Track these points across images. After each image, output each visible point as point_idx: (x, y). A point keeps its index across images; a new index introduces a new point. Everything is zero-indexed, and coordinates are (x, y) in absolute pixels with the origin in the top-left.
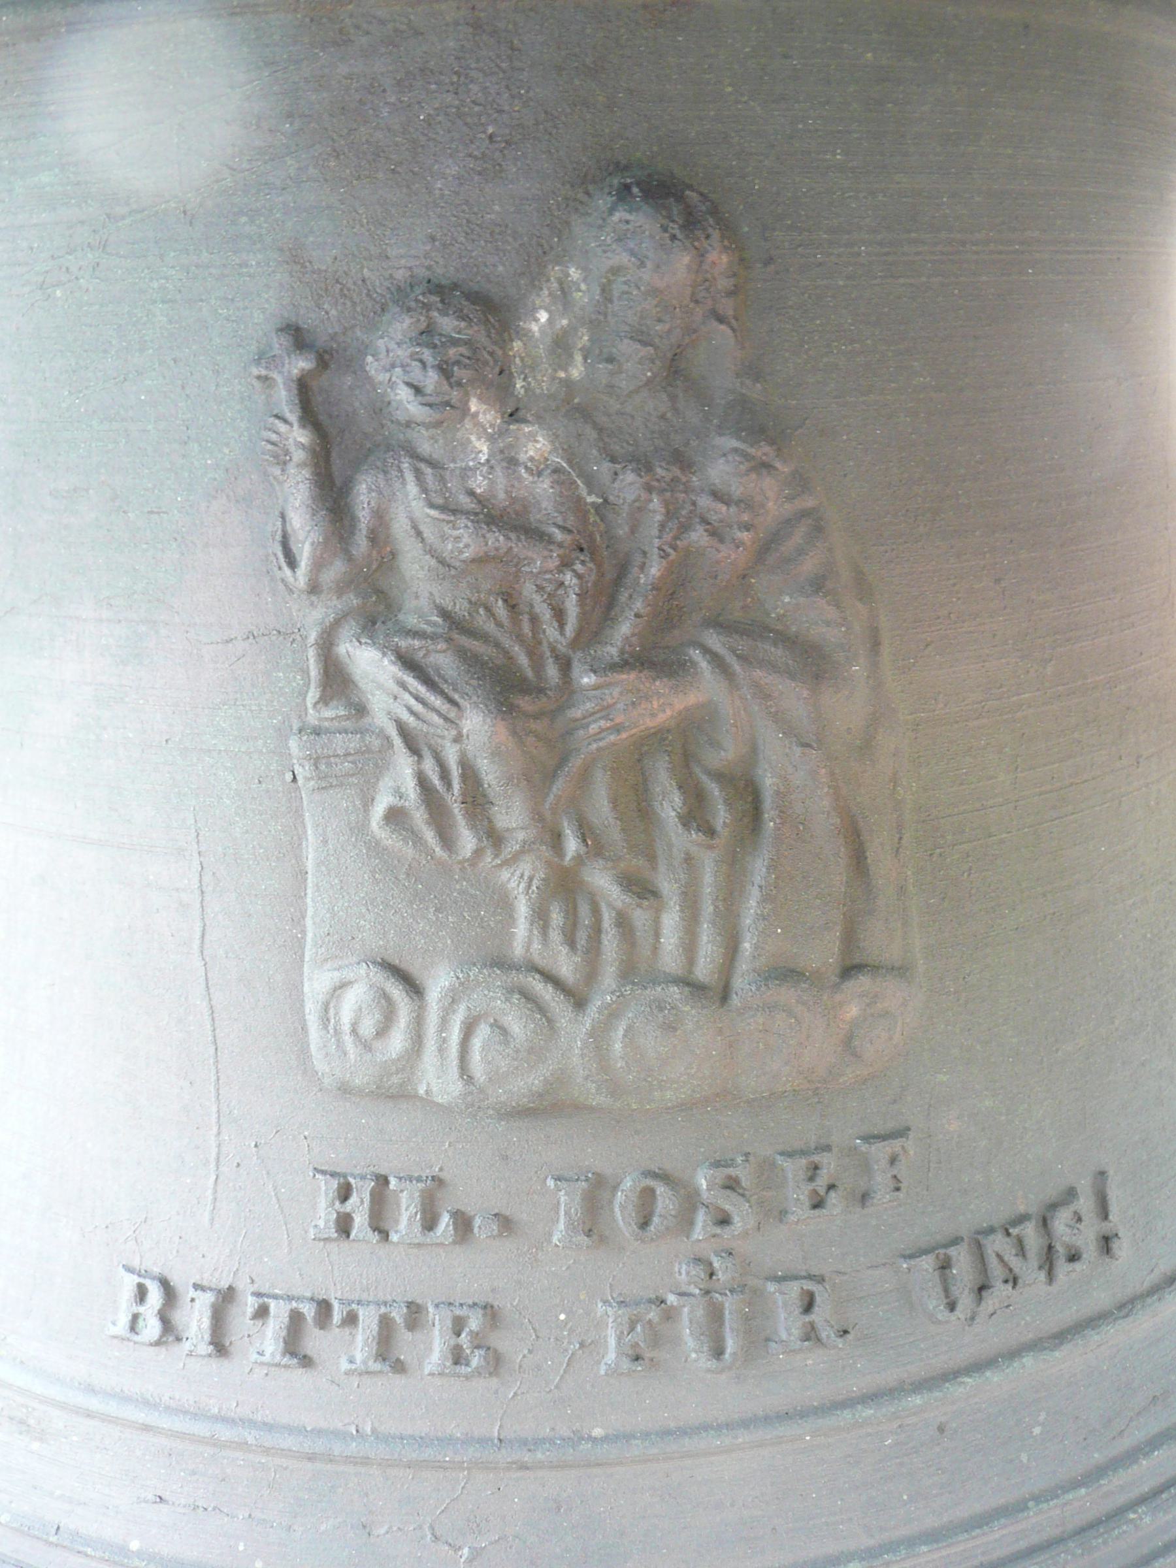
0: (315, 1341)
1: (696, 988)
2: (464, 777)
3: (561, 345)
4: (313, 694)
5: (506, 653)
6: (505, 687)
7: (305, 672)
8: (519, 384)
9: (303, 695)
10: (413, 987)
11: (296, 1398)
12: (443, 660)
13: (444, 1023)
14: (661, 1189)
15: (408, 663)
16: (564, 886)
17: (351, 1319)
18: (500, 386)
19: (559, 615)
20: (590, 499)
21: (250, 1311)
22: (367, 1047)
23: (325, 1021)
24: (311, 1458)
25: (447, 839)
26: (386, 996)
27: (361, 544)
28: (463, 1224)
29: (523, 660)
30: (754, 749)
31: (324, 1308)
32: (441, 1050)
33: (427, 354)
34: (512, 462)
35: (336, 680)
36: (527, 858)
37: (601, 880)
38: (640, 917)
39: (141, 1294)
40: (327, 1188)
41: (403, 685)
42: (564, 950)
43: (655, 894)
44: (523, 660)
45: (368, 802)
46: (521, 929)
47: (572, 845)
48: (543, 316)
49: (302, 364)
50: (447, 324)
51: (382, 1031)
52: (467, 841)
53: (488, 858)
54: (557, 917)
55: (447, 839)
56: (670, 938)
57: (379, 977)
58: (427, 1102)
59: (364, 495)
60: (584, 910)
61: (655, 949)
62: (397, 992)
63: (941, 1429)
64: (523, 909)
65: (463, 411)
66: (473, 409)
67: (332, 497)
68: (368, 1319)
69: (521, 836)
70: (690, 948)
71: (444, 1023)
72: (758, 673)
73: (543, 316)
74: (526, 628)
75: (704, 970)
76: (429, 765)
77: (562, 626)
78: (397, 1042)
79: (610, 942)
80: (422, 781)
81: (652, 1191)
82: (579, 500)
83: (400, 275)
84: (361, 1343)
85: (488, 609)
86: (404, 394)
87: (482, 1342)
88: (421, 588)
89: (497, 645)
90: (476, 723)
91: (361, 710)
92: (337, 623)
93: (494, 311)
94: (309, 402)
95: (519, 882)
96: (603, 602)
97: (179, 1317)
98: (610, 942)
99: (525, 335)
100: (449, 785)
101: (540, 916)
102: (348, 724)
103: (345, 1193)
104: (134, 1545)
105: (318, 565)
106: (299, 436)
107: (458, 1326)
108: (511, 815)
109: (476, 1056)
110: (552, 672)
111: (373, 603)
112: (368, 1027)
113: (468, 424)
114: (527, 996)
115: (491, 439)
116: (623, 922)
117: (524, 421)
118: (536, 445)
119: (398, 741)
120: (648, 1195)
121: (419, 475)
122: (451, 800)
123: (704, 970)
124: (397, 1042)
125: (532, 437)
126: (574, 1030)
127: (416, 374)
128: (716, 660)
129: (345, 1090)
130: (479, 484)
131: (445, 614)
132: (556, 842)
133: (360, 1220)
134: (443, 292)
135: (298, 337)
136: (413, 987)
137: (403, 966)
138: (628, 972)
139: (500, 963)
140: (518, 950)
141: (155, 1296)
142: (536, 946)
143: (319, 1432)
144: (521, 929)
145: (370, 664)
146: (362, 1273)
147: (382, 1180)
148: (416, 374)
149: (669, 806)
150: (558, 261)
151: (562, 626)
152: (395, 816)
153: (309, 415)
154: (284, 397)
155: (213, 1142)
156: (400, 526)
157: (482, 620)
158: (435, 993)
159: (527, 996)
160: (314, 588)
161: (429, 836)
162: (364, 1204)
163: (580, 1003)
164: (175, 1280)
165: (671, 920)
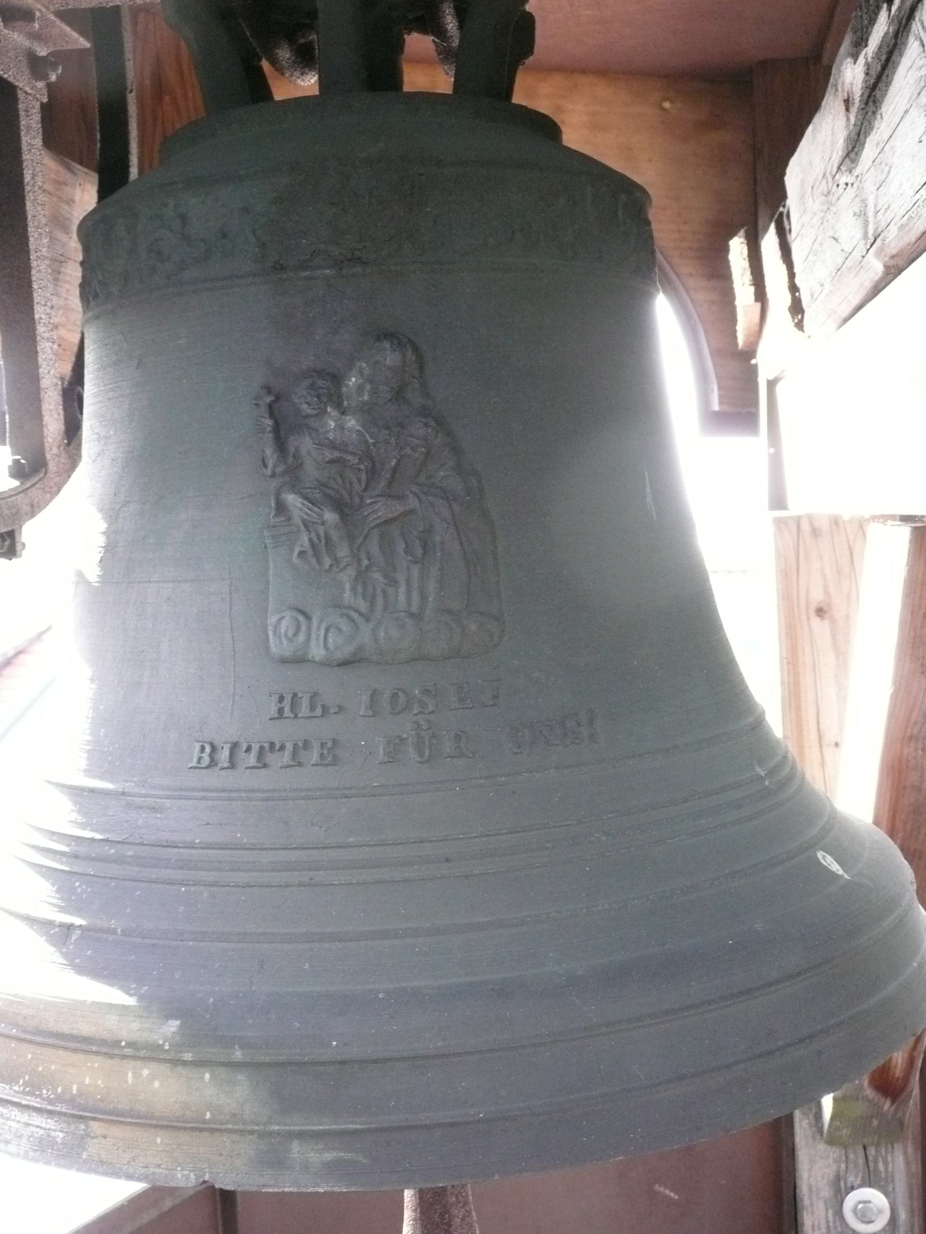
0: (270, 758)
1: (412, 615)
2: (326, 538)
3: (360, 388)
4: (273, 513)
5: (341, 495)
6: (340, 507)
7: (270, 507)
8: (346, 403)
9: (269, 515)
10: (308, 617)
11: (262, 780)
12: (317, 495)
13: (319, 628)
14: (400, 694)
15: (306, 498)
16: (361, 577)
17: (282, 748)
18: (339, 406)
19: (359, 480)
20: (371, 441)
21: (244, 748)
22: (290, 640)
23: (275, 633)
24: (266, 800)
25: (319, 562)
26: (297, 620)
27: (290, 460)
28: (325, 709)
29: (347, 496)
30: (431, 526)
31: (272, 745)
32: (317, 639)
33: (313, 393)
34: (342, 428)
35: (281, 508)
36: (349, 568)
37: (377, 576)
38: (390, 590)
39: (203, 749)
40: (275, 698)
41: (304, 504)
42: (362, 601)
43: (396, 582)
44: (347, 496)
45: (292, 551)
46: (347, 595)
47: (365, 562)
48: (354, 379)
49: (269, 399)
50: (320, 382)
51: (296, 634)
52: (327, 562)
53: (335, 569)
54: (360, 589)
55: (319, 562)
56: (402, 598)
57: (294, 613)
58: (313, 662)
59: (293, 443)
60: (370, 588)
61: (397, 601)
62: (301, 618)
63: (514, 793)
64: (348, 587)
65: (325, 411)
66: (329, 410)
67: (281, 445)
68: (289, 746)
69: (346, 559)
70: (409, 601)
71: (319, 628)
72: (430, 498)
73: (354, 379)
74: (348, 485)
75: (414, 609)
76: (313, 535)
77: (360, 485)
78: (301, 637)
79: (380, 600)
80: (311, 540)
81: (397, 694)
82: (367, 441)
83: (305, 368)
84: (286, 757)
85: (334, 479)
86: (305, 406)
87: (331, 754)
88: (311, 472)
89: (338, 492)
90: (330, 516)
91: (289, 519)
92: (281, 487)
93: (337, 379)
94: (271, 410)
95: (346, 577)
96: (373, 473)
97: (217, 757)
98: (380, 600)
99: (347, 386)
100: (320, 541)
101: (353, 589)
102: (285, 524)
103: (281, 699)
104: (197, 841)
105: (275, 467)
106: (269, 422)
107: (323, 745)
108: (343, 551)
109: (330, 640)
110: (357, 500)
111: (292, 475)
112: (290, 633)
113: (327, 415)
114: (349, 617)
115: (335, 421)
116: (384, 592)
117: (348, 415)
118: (351, 422)
119: (302, 527)
120: (395, 695)
121: (310, 435)
122: (321, 547)
123: (414, 609)
124: (301, 637)
125: (350, 420)
126: (366, 630)
127: (309, 399)
128: (415, 494)
129: (283, 661)
130: (331, 436)
131: (318, 481)
132: (359, 561)
133: (287, 712)
134: (320, 373)
135: (269, 390)
136: (308, 617)
137: (301, 608)
138: (385, 609)
139: (339, 606)
140: (346, 602)
141: (208, 749)
142: (353, 600)
143: (269, 791)
144: (347, 595)
145: (291, 499)
146: (288, 732)
147: (295, 695)
148: (309, 399)
149: (401, 547)
150: (359, 360)
151: (360, 485)
152: (302, 554)
153: (272, 415)
154: (264, 410)
155: (232, 688)
156: (304, 452)
157: (332, 483)
158: (315, 622)
159: (349, 617)
160: (273, 475)
161: (314, 561)
162: (288, 705)
163: (367, 620)
164: (216, 743)
165: (402, 590)
